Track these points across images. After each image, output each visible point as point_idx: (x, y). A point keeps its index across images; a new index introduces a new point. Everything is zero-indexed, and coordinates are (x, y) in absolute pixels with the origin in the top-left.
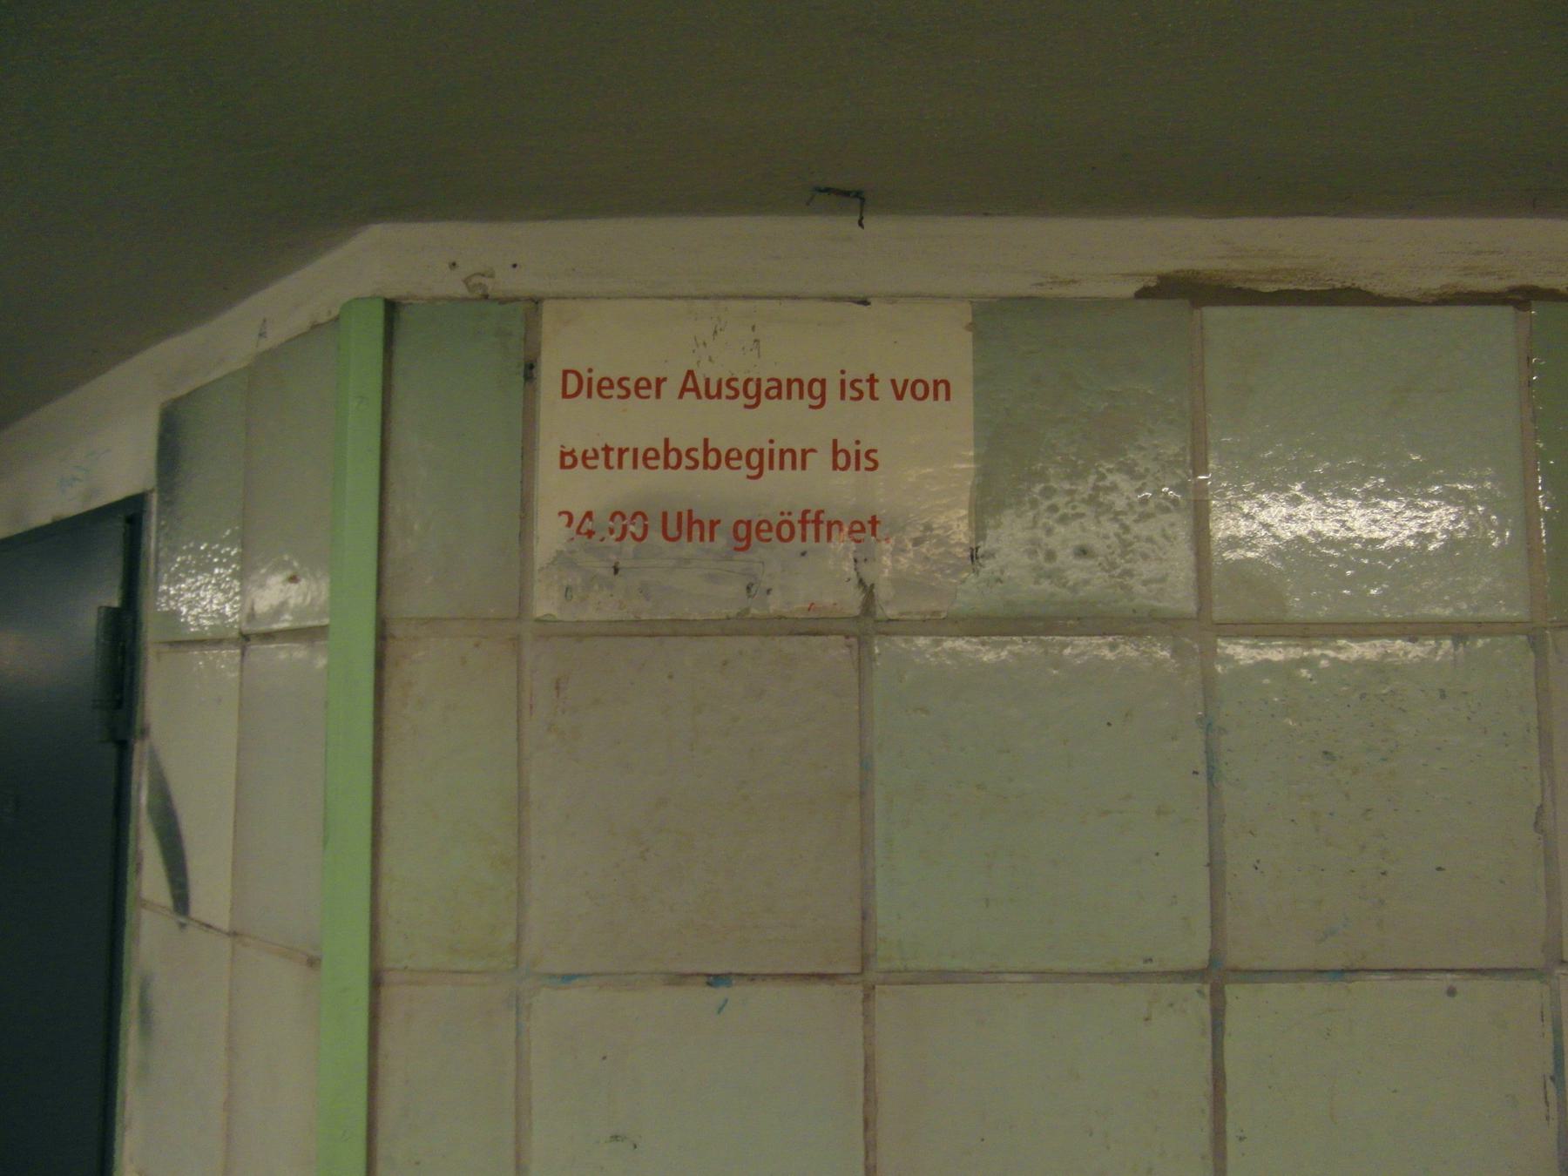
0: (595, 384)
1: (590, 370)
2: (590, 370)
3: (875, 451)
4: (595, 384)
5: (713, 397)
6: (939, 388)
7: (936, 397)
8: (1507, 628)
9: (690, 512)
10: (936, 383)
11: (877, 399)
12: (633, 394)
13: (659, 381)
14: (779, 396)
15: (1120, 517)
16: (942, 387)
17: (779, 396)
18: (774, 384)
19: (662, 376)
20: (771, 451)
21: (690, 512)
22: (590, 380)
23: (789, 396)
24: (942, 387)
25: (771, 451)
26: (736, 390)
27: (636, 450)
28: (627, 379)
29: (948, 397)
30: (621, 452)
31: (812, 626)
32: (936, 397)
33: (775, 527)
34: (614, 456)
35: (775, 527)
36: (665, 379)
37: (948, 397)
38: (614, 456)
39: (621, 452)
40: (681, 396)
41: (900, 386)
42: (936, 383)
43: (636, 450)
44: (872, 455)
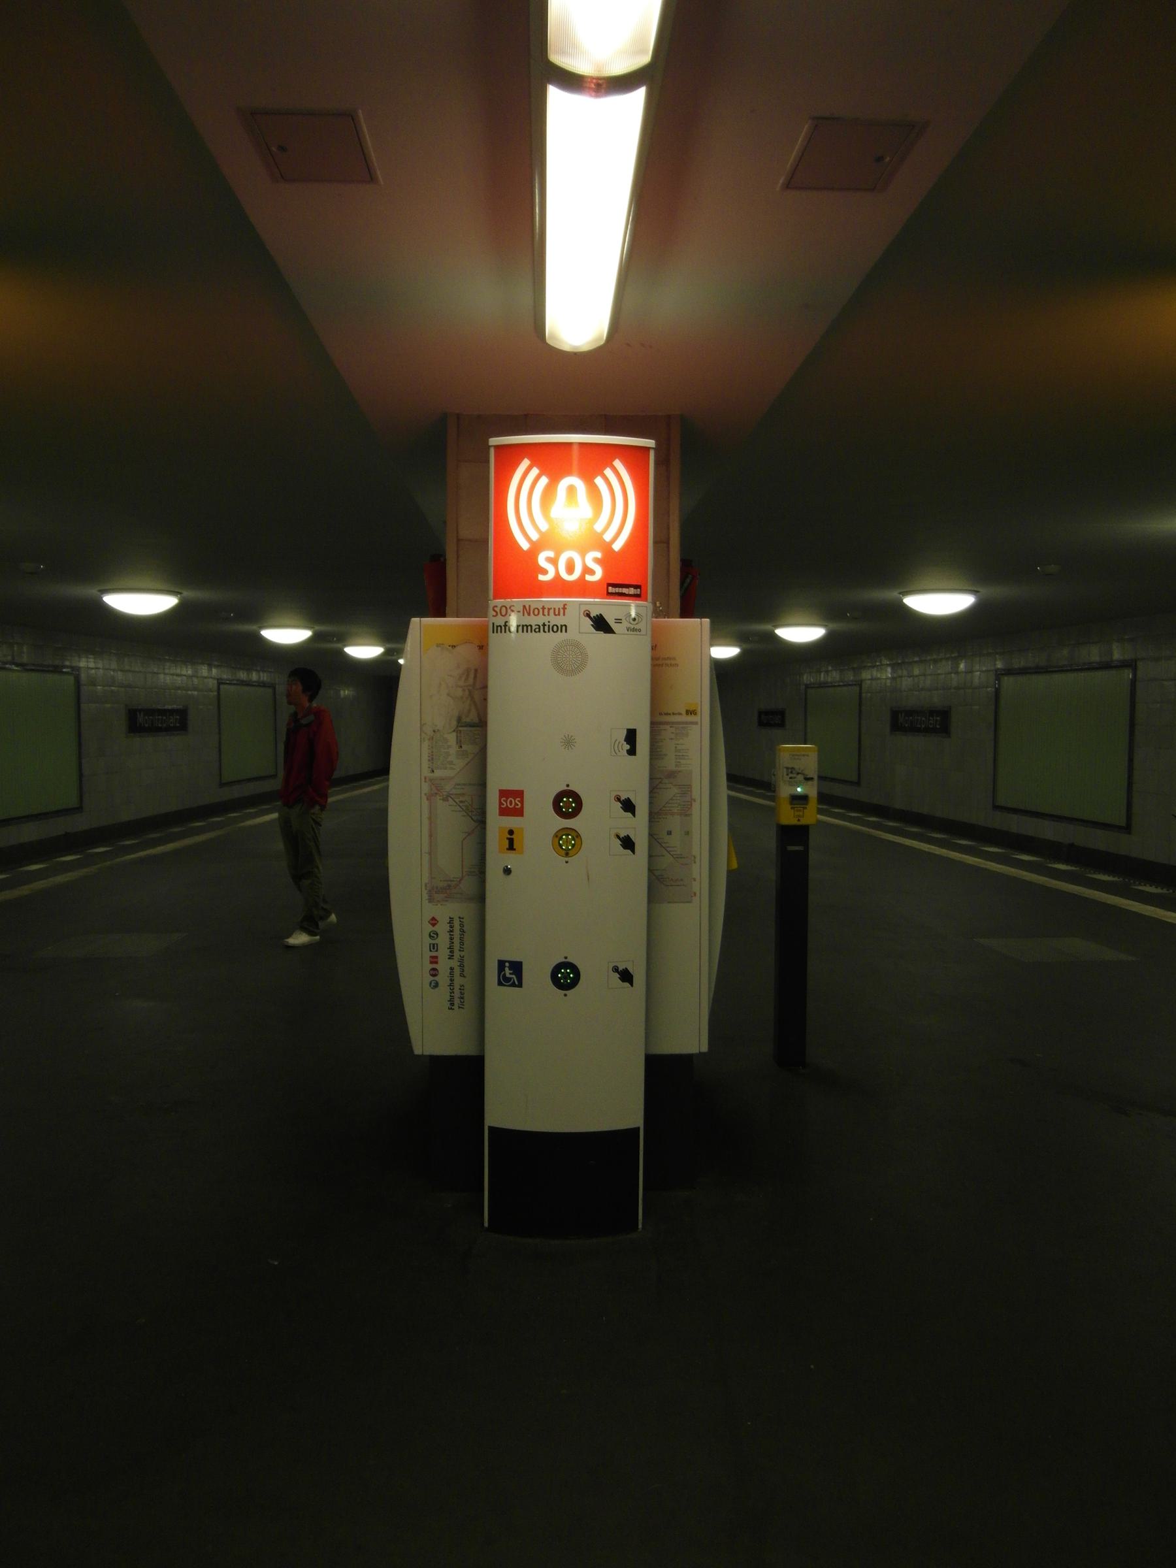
3: (513, 606)
6: (812, 779)
7: (561, 631)
8: (572, 81)
10: (562, 626)
11: (515, 850)
12: (508, 607)
14: (539, 631)
16: (564, 628)
24: (564, 628)
26: (494, 610)
27: (554, 609)
28: (496, 606)
29: (566, 631)
30: (549, 609)
31: (870, 692)
32: (561, 631)
34: (546, 611)
37: (566, 631)
38: (546, 611)
39: (549, 609)
42: (562, 626)
43: (554, 609)
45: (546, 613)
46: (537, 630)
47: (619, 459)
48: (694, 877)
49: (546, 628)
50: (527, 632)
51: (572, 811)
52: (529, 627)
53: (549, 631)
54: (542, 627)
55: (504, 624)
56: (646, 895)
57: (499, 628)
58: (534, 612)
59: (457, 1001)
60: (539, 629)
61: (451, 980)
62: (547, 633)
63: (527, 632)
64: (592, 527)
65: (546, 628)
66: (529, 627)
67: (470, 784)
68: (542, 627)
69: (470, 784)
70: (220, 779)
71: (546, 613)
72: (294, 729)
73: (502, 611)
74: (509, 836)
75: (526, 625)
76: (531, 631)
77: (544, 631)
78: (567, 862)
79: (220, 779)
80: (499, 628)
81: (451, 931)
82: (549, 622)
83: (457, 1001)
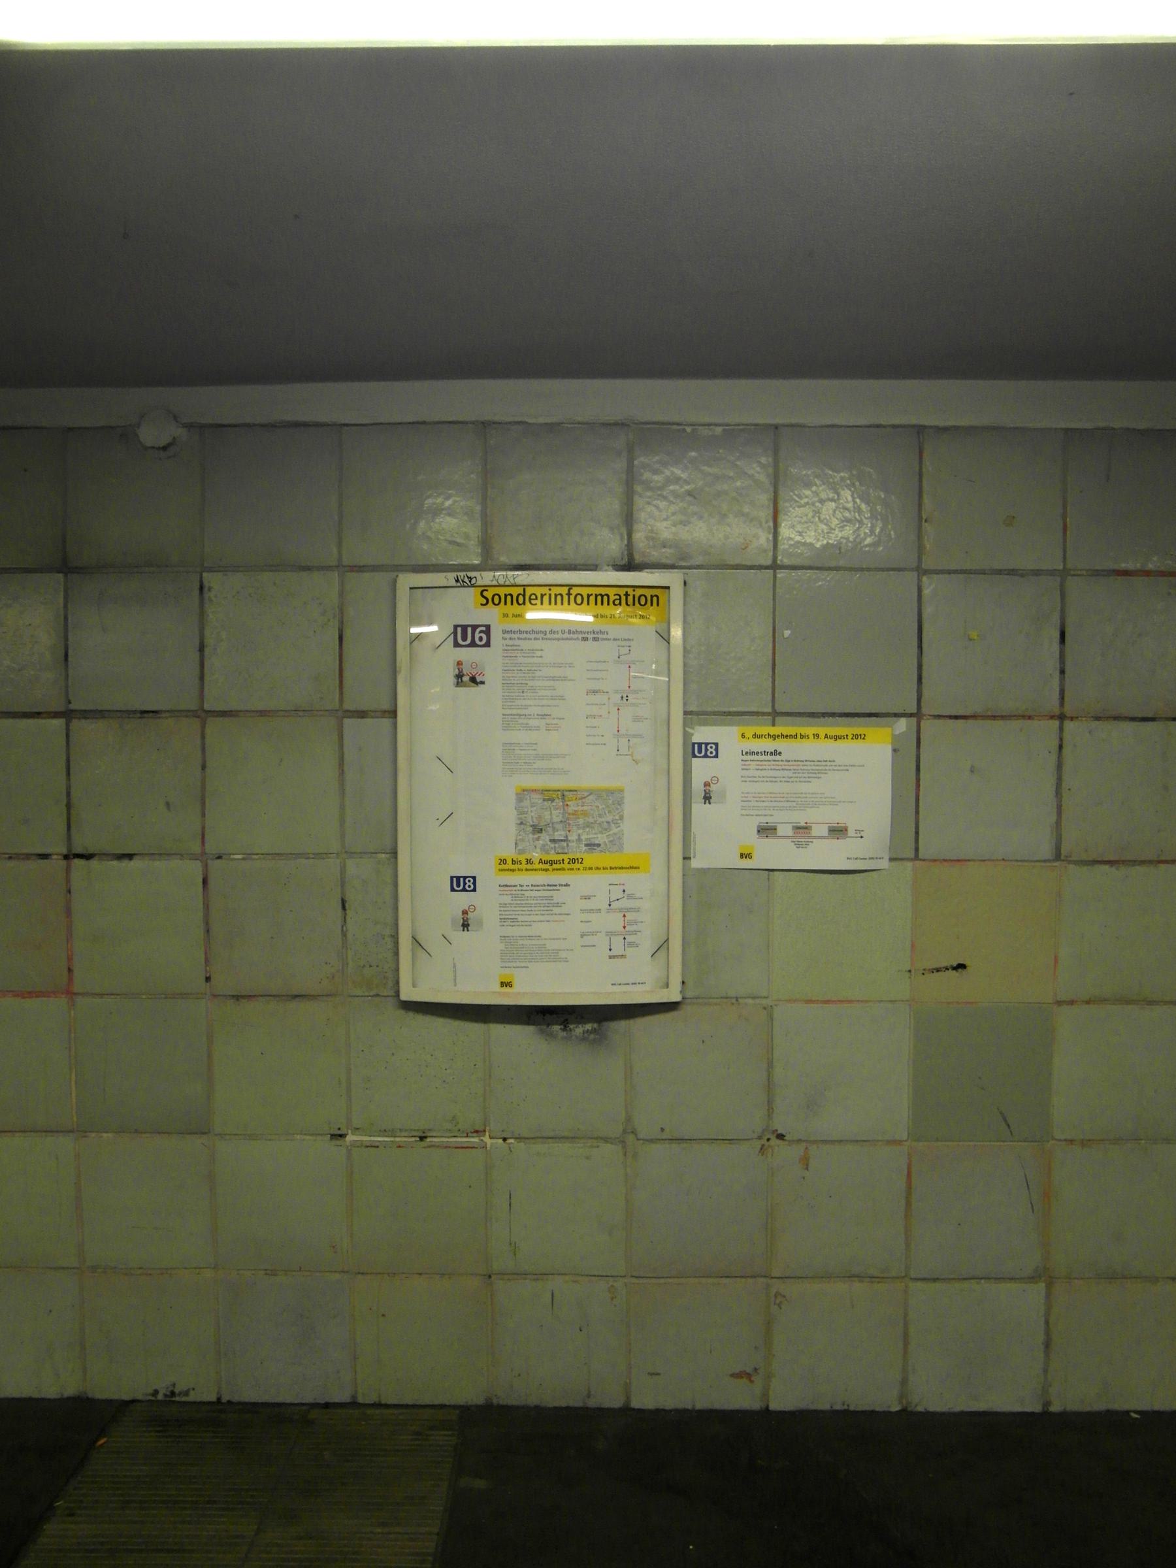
14: (620, 604)
46: (617, 602)
48: (765, 1012)
49: (630, 599)
50: (602, 604)
51: (688, 1547)
52: (605, 598)
53: (634, 605)
54: (623, 598)
57: (559, 598)
60: (620, 599)
63: (602, 604)
64: (400, 1000)
65: (630, 599)
66: (605, 598)
68: (623, 598)
72: (205, 817)
74: (599, 615)
75: (601, 595)
77: (503, 724)
80: (559, 598)
81: (594, 633)
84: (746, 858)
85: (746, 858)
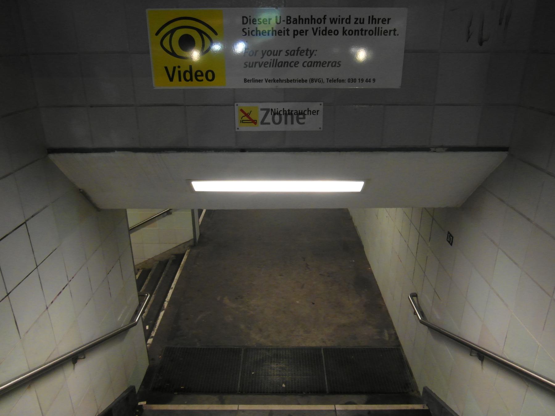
0: (250, 32)
1: (277, 109)
2: (277, 109)
3: (244, 67)
4: (250, 32)
5: (280, 67)
9: (373, 16)
11: (289, 35)
13: (318, 111)
14: (296, 23)
15: (119, 261)
17: (296, 23)
18: (296, 111)
19: (281, 49)
20: (339, 19)
21: (373, 16)
22: (250, 19)
23: (299, 23)
25: (339, 19)
30: (366, 31)
32: (355, 35)
33: (333, 31)
34: (363, 32)
35: (333, 31)
36: (308, 30)
38: (363, 32)
40: (350, 16)
41: (266, 79)
44: (245, 66)
45: (295, 81)
47: (364, 183)
55: (297, 49)
56: (177, 26)
58: (354, 81)
59: (274, 65)
61: (291, 81)
62: (364, 36)
67: (526, 392)
69: (526, 392)
70: (26, 226)
71: (295, 81)
73: (292, 53)
76: (360, 19)
78: (324, 82)
79: (26, 226)
82: (250, 17)
83: (274, 65)
84: (316, 82)
85: (316, 82)
